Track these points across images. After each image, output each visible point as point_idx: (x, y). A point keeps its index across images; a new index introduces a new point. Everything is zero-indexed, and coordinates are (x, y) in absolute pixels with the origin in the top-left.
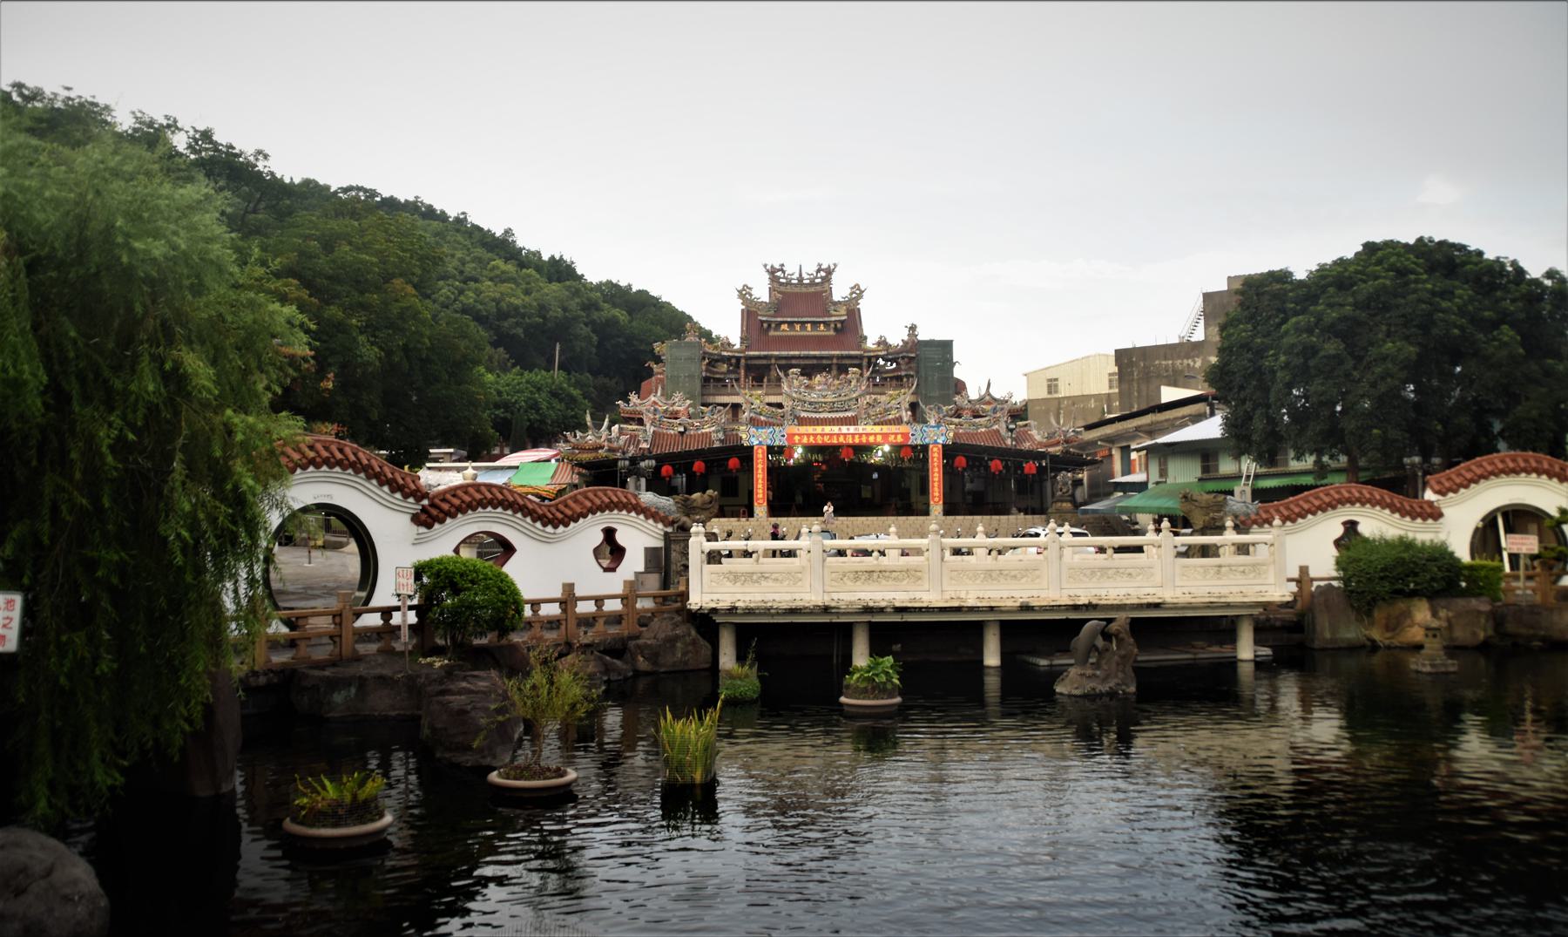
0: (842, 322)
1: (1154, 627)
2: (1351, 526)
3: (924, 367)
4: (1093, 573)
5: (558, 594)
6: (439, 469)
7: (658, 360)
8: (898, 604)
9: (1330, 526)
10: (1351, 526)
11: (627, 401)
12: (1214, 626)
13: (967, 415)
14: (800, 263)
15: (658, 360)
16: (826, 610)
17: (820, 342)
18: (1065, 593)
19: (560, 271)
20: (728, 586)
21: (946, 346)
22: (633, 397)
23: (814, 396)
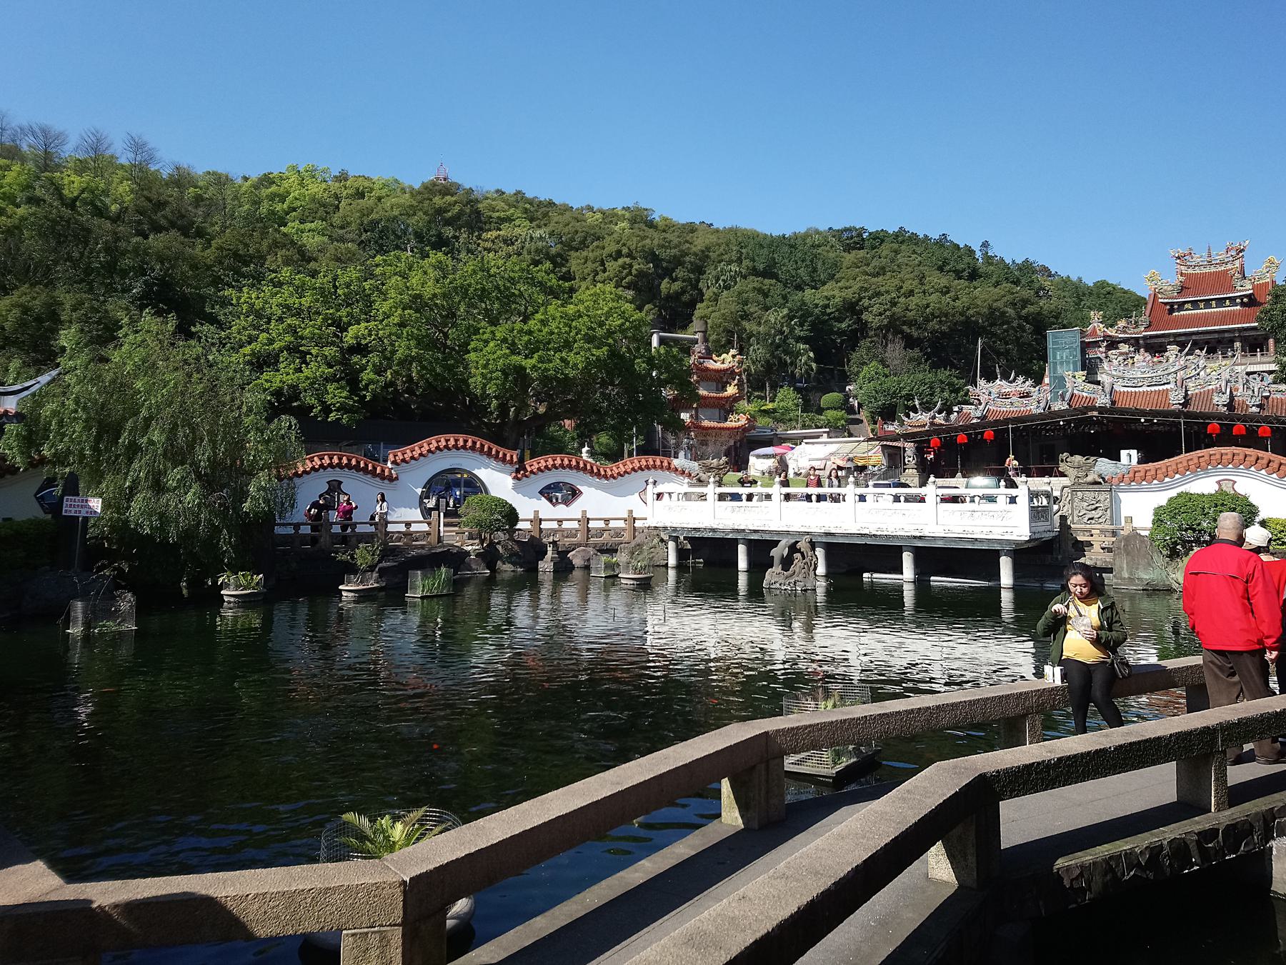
17: (1224, 318)
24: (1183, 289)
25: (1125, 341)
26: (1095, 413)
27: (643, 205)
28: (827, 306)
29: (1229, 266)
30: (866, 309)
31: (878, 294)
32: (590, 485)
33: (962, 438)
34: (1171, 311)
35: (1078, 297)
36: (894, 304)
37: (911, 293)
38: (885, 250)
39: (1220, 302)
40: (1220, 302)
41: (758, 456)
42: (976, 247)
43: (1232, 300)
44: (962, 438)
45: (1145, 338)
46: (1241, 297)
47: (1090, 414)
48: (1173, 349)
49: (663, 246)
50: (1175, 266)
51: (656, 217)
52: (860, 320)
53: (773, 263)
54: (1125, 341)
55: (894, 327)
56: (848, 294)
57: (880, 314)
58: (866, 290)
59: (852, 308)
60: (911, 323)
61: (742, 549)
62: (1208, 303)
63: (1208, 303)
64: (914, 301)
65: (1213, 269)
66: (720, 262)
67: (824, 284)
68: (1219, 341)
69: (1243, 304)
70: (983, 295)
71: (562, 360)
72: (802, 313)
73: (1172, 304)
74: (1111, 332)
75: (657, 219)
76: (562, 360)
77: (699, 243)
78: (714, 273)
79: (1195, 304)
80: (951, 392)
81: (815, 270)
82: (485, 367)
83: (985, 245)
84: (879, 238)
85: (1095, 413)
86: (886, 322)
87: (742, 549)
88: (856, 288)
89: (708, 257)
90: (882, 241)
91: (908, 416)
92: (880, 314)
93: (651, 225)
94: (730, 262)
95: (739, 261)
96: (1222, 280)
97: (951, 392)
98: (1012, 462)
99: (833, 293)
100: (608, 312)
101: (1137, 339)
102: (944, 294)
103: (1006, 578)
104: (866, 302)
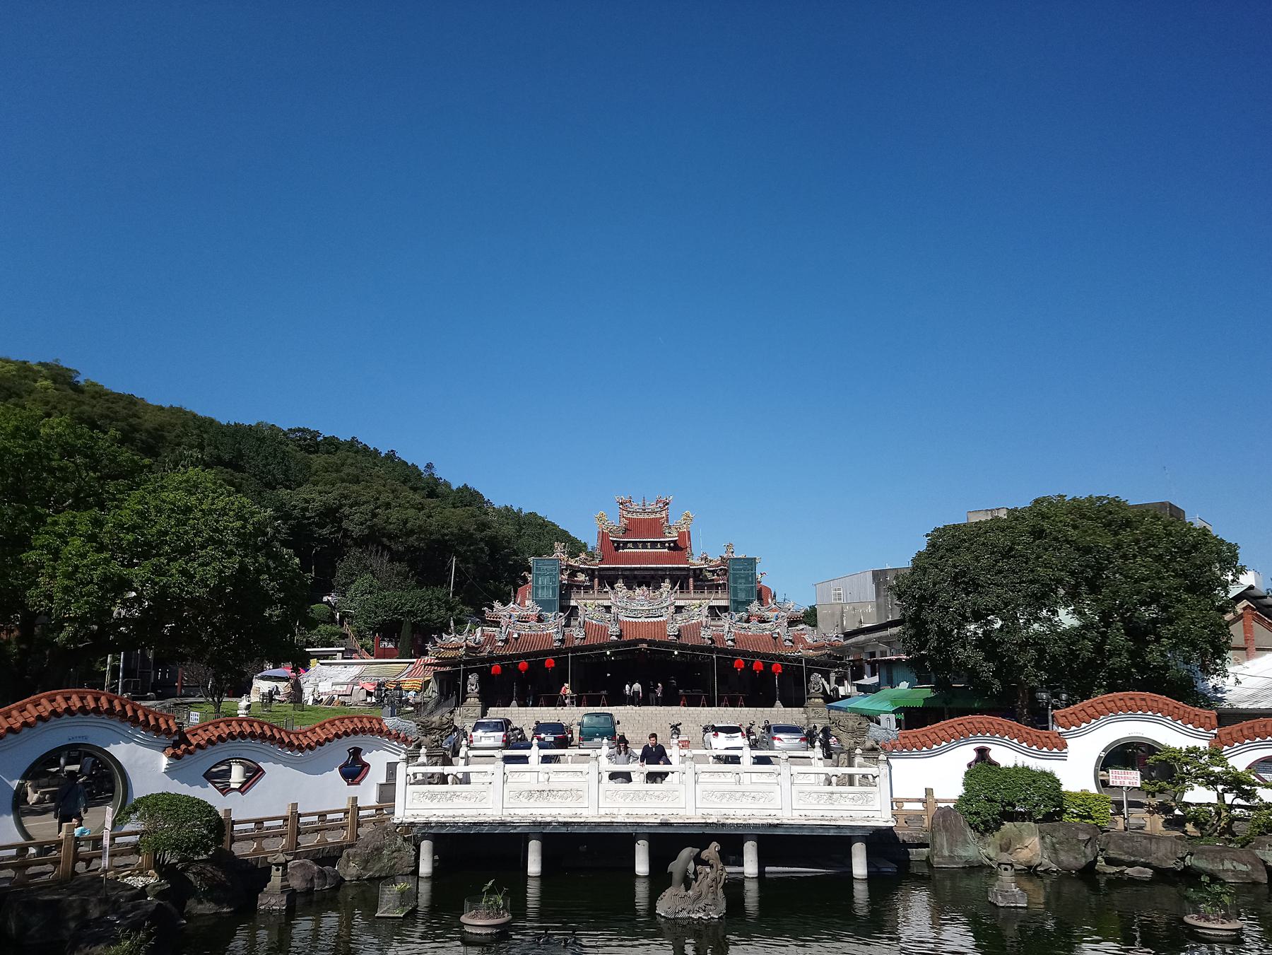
0: (674, 542)
1: (778, 843)
2: (982, 753)
3: (737, 582)
4: (723, 796)
5: (285, 812)
6: (330, 664)
7: (529, 570)
8: (561, 820)
9: (966, 753)
10: (982, 753)
11: (492, 608)
12: (827, 846)
13: (754, 621)
14: (644, 502)
15: (529, 570)
16: (503, 824)
17: (658, 558)
18: (699, 812)
19: (469, 498)
20: (428, 804)
21: (752, 562)
22: (497, 604)
23: (634, 606)
24: (626, 531)
25: (582, 571)
26: (645, 646)
27: (65, 364)
28: (306, 509)
29: (658, 516)
30: (347, 517)
31: (356, 504)
32: (276, 761)
33: (523, 665)
34: (617, 549)
35: (519, 525)
36: (374, 515)
37: (388, 506)
38: (341, 454)
39: (654, 545)
40: (654, 545)
41: (263, 678)
42: (422, 468)
43: (663, 543)
44: (523, 665)
45: (600, 569)
46: (669, 542)
47: (640, 646)
48: (666, 585)
49: (107, 417)
50: (617, 510)
51: (81, 380)
52: (340, 528)
53: (240, 455)
54: (582, 571)
55: (374, 539)
56: (331, 499)
57: (362, 524)
58: (346, 497)
59: (331, 514)
60: (391, 537)
61: (534, 848)
62: (644, 545)
63: (644, 545)
64: (395, 515)
65: (646, 517)
66: (179, 444)
67: (300, 485)
68: (653, 577)
69: (670, 548)
70: (455, 518)
71: (184, 572)
72: (283, 513)
73: (619, 543)
74: (572, 562)
75: (82, 383)
76: (184, 572)
77: (149, 422)
78: (172, 457)
79: (635, 544)
80: (447, 610)
81: (288, 469)
82: (69, 576)
83: (429, 466)
84: (332, 444)
85: (645, 646)
86: (366, 532)
87: (534, 848)
88: (335, 493)
89: (163, 437)
90: (337, 448)
91: (441, 637)
92: (362, 524)
93: (77, 388)
94: (191, 447)
95: (201, 447)
96: (655, 526)
97: (447, 610)
98: (567, 689)
99: (310, 497)
100: (224, 509)
101: (593, 570)
102: (420, 510)
103: (859, 868)
104: (346, 510)
